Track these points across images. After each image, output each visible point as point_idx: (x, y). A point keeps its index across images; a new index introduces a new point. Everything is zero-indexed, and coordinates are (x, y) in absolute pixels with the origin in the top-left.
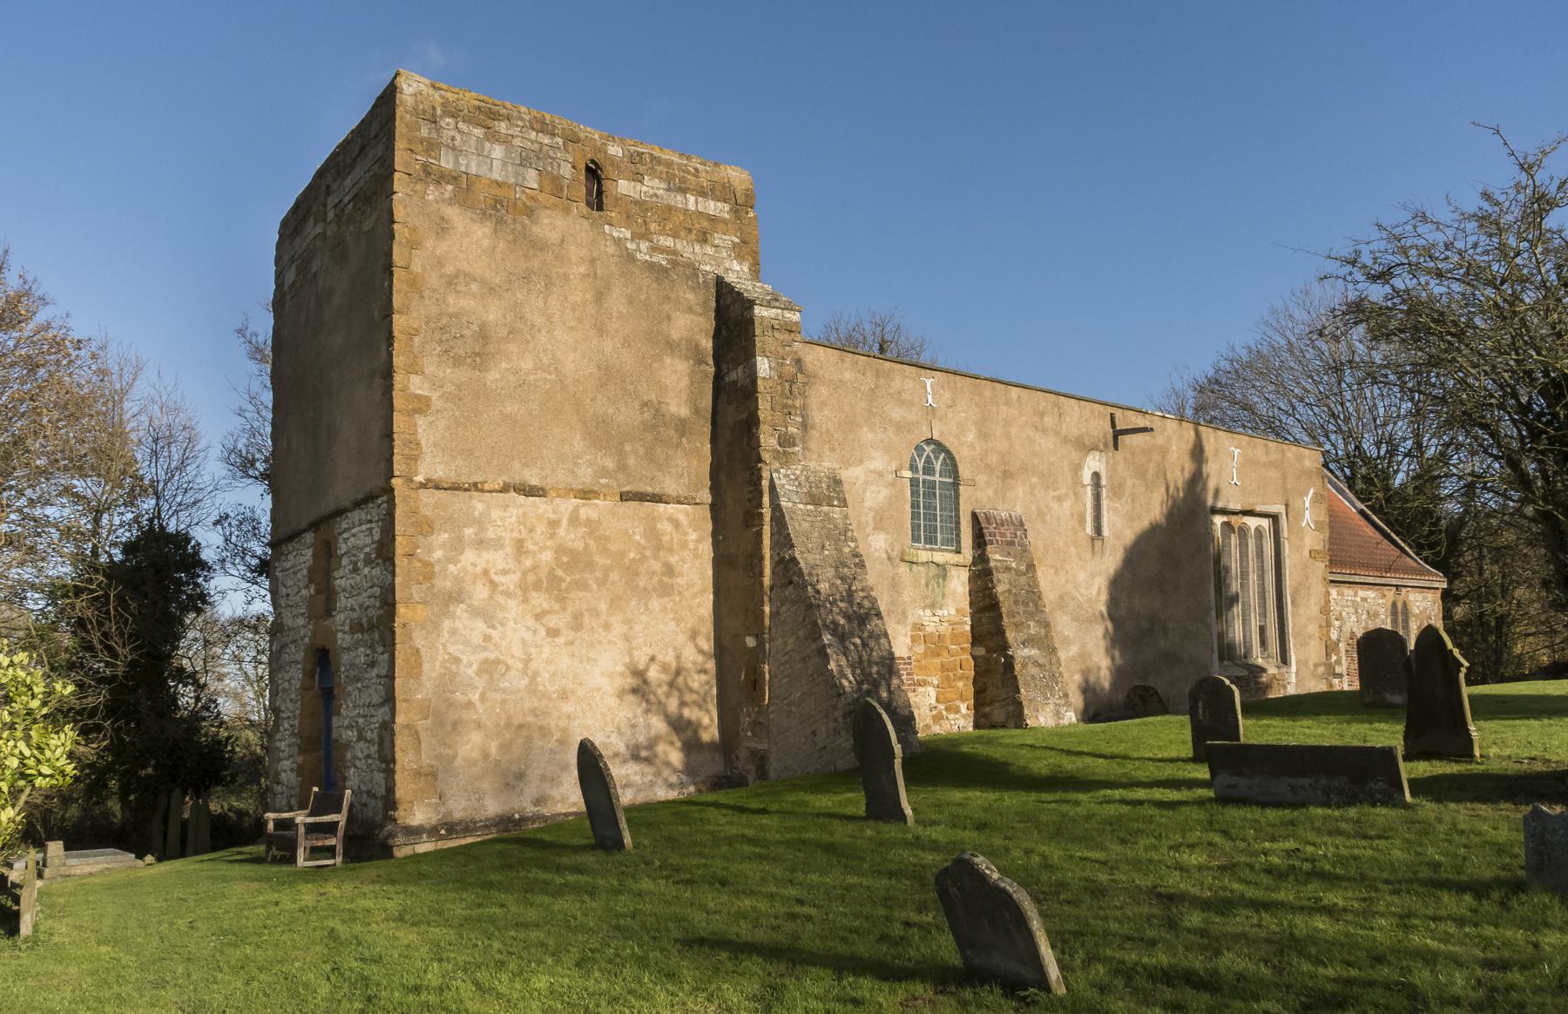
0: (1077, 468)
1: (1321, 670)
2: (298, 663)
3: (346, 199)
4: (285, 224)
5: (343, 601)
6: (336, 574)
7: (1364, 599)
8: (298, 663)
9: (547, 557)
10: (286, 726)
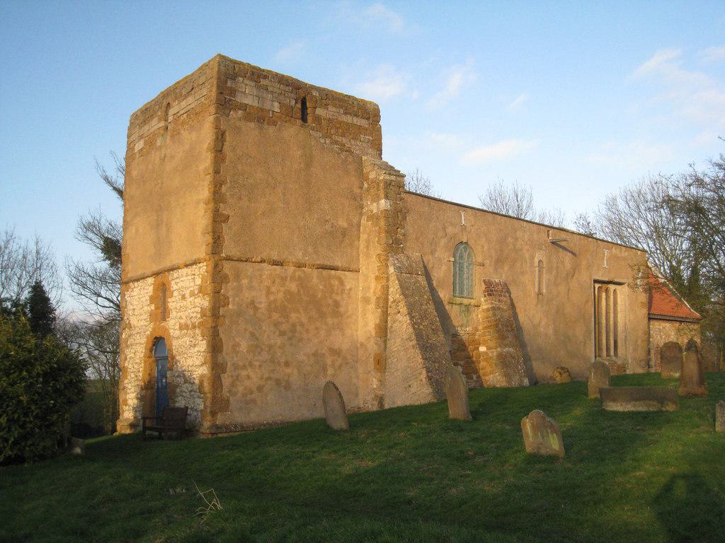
0: (532, 258)
1: (643, 363)
2: (142, 344)
3: (183, 112)
4: (135, 117)
5: (173, 314)
6: (169, 300)
7: (664, 328)
8: (142, 344)
9: (281, 295)
10: (133, 376)
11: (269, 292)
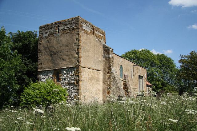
11: (89, 76)
